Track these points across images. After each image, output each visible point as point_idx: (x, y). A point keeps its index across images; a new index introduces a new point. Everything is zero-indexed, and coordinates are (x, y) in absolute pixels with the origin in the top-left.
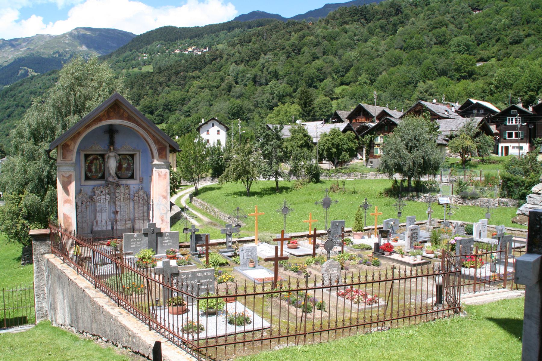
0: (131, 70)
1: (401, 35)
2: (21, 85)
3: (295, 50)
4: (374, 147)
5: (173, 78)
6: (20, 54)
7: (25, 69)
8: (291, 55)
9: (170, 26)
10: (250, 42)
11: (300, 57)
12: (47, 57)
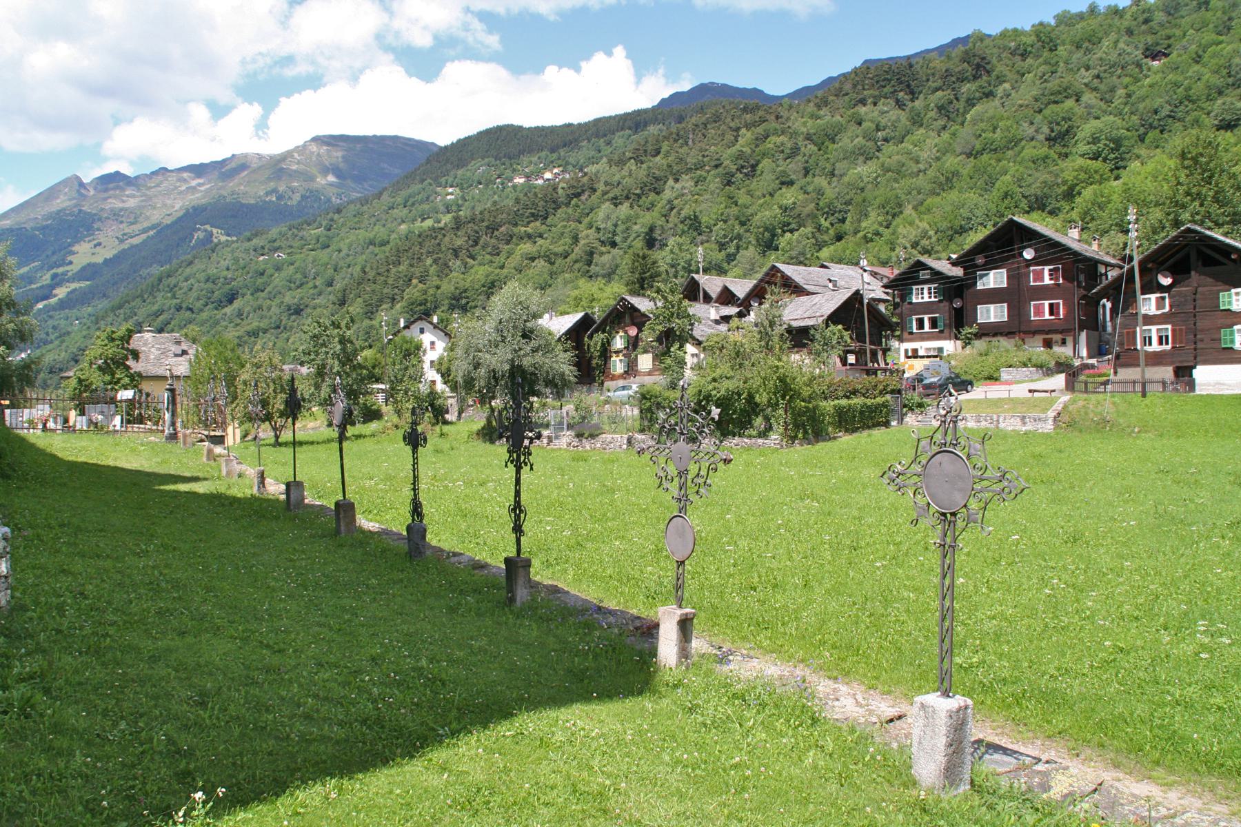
0: (418, 224)
1: (974, 122)
2: (191, 263)
3: (743, 167)
4: (611, 357)
5: (484, 239)
6: (198, 199)
7: (206, 231)
8: (733, 180)
9: (508, 126)
10: (658, 152)
11: (754, 184)
12: (252, 202)
